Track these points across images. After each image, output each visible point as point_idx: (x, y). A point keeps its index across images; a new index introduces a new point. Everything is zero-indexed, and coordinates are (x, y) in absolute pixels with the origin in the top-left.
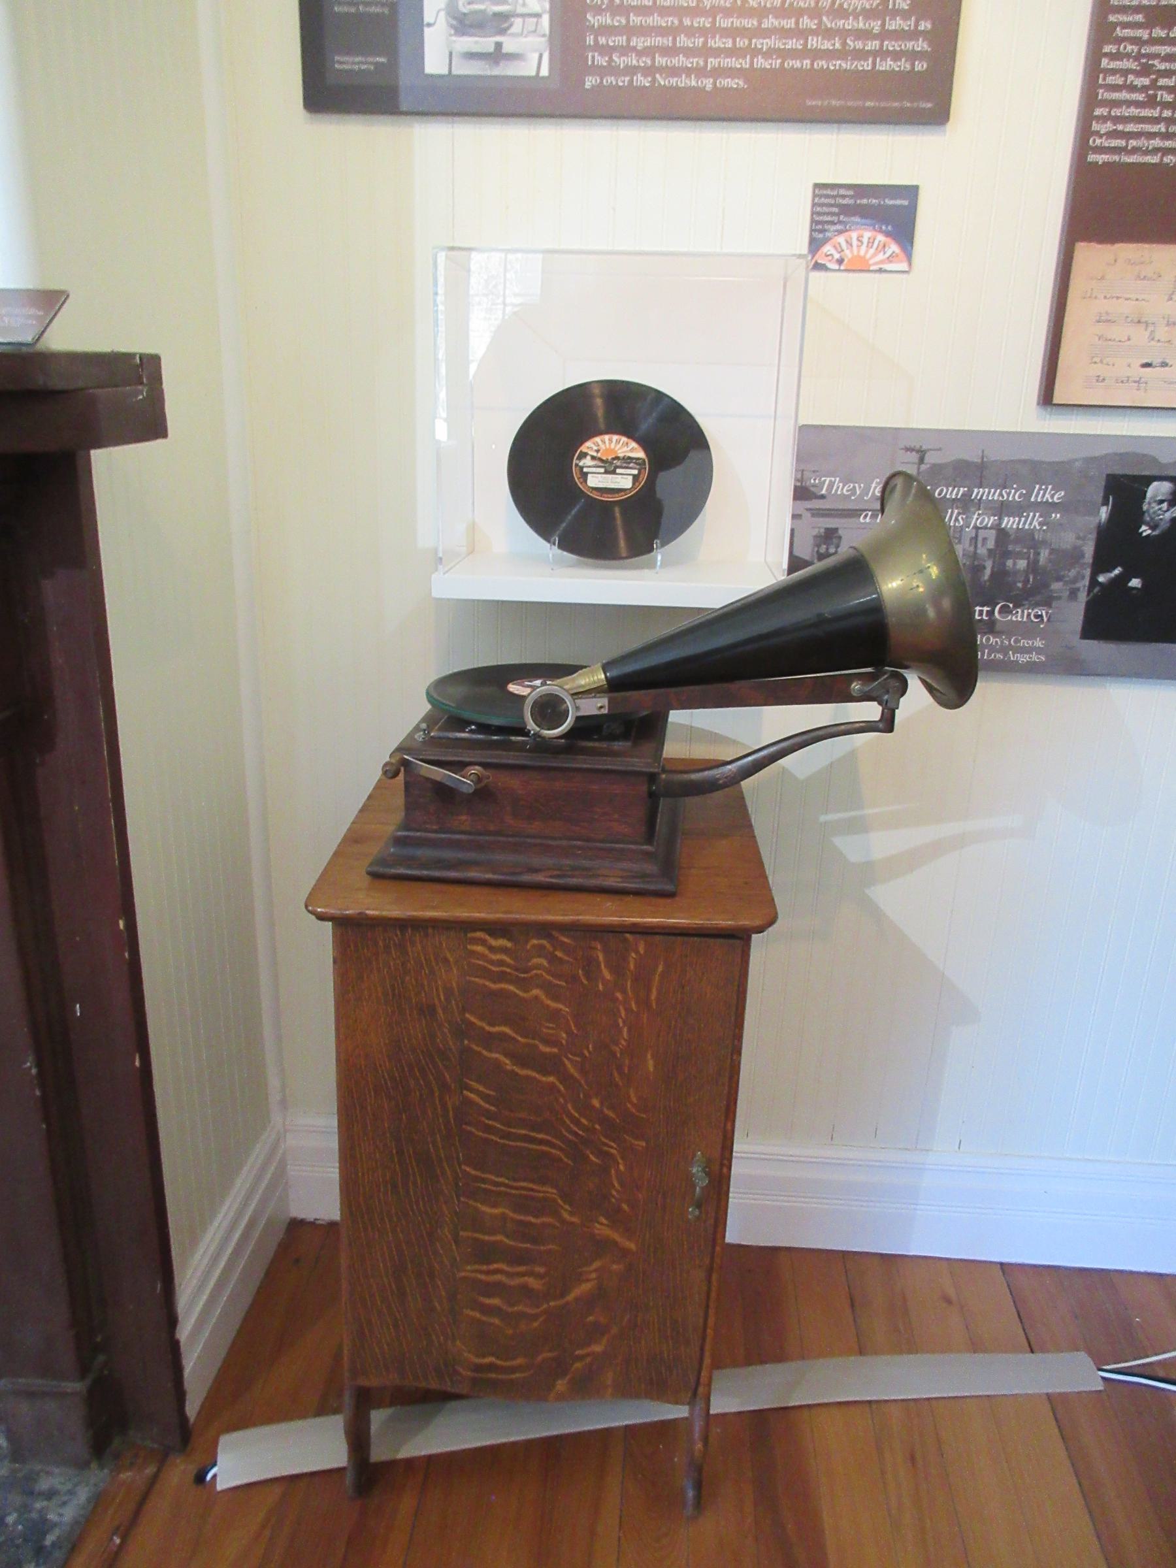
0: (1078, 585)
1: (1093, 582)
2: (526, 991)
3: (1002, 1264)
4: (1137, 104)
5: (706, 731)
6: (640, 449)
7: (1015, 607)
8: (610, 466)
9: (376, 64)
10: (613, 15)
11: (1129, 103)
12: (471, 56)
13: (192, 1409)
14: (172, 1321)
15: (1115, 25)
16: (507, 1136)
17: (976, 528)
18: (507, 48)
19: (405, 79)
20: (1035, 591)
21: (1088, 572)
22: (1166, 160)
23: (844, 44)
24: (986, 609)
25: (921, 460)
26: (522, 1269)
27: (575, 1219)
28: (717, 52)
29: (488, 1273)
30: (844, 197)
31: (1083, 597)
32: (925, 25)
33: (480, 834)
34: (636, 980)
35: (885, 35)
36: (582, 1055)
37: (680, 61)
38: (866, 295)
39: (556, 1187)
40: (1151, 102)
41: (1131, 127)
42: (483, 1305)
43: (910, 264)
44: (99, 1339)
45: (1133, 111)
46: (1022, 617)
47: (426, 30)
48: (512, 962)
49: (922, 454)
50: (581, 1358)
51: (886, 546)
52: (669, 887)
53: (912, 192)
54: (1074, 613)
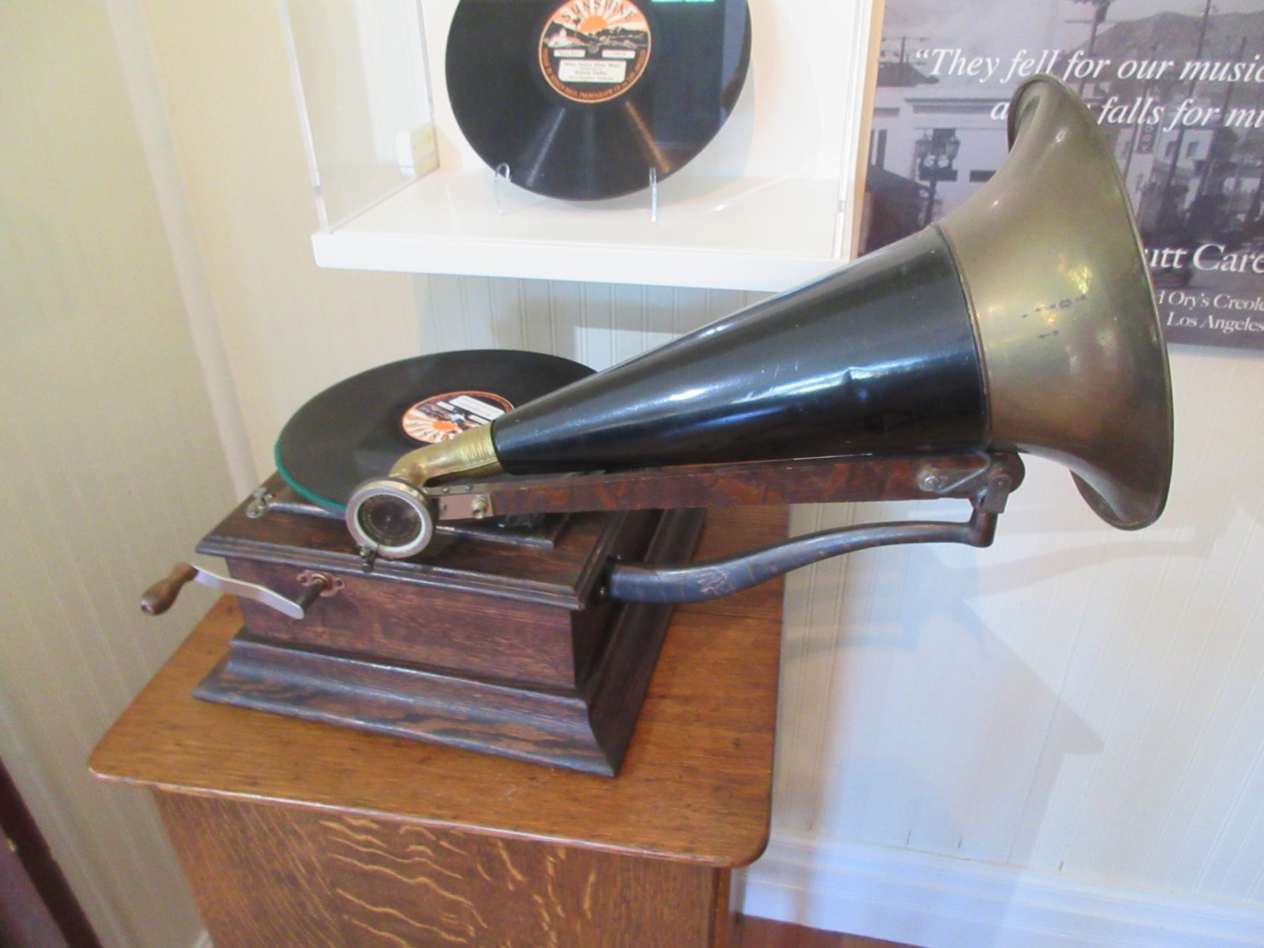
6: (642, 17)
17: (1181, 128)
24: (1179, 253)
34: (559, 887)
46: (1238, 265)
48: (385, 846)
51: (997, 237)
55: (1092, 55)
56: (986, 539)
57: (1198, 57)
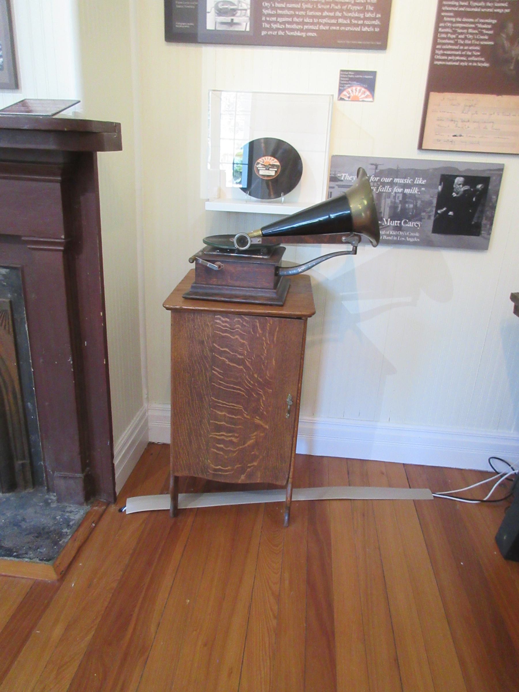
0: (431, 214)
1: (436, 213)
2: (234, 336)
3: (404, 464)
4: (451, 44)
5: (297, 255)
8: (268, 167)
9: (190, 26)
10: (272, 10)
12: (223, 23)
13: (118, 490)
14: (112, 456)
15: (443, 17)
16: (227, 387)
17: (395, 193)
18: (235, 21)
19: (200, 32)
20: (416, 216)
21: (434, 209)
23: (351, 21)
25: (376, 168)
26: (230, 434)
27: (248, 417)
28: (307, 24)
29: (219, 435)
30: (350, 75)
31: (433, 218)
32: (379, 16)
33: (219, 285)
34: (269, 333)
35: (365, 19)
36: (251, 359)
37: (294, 26)
39: (242, 405)
40: (456, 44)
41: (449, 52)
42: (217, 447)
43: (373, 98)
44: (88, 461)
47: (208, 15)
49: (377, 166)
50: (250, 467)
52: (281, 303)
53: (374, 73)
54: (430, 224)
55: (376, 176)
56: (355, 253)
57: (397, 178)
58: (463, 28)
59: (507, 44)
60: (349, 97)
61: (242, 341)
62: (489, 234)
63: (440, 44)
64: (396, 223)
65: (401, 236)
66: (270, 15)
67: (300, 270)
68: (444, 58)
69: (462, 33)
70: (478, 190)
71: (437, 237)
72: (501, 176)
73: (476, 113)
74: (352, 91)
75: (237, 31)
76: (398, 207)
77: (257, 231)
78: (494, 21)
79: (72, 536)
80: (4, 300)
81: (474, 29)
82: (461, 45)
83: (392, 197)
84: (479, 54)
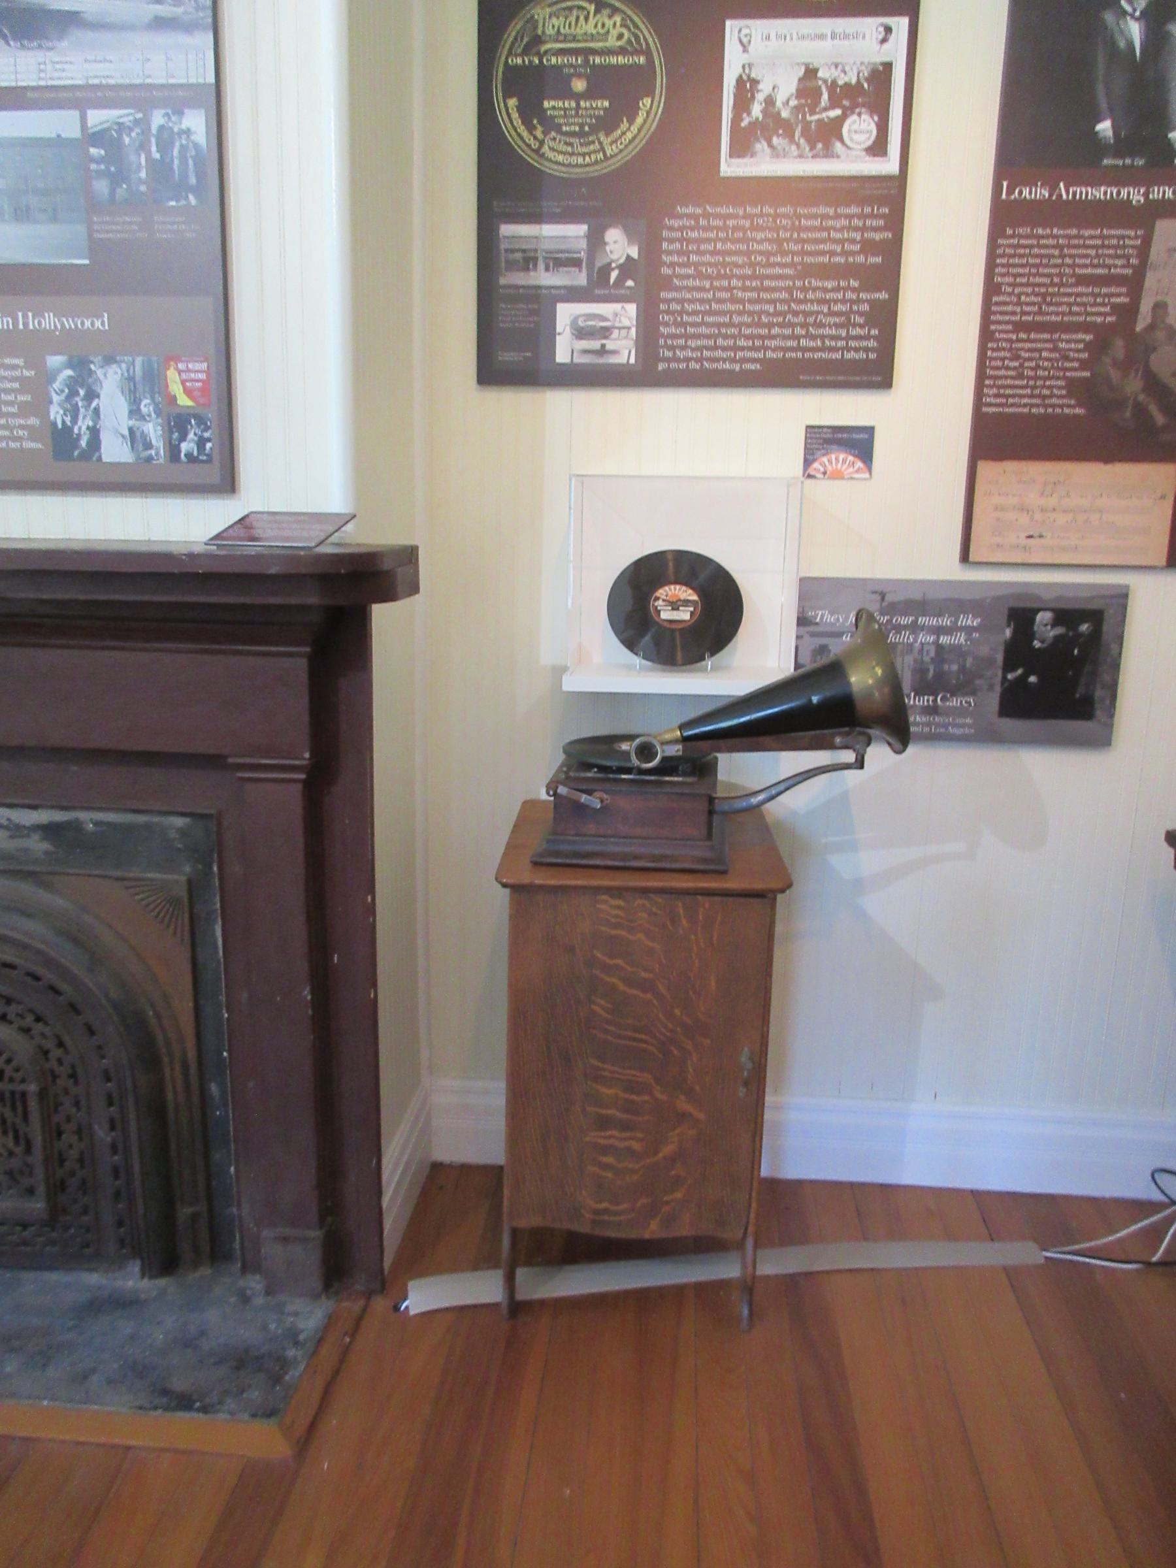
1: (1004, 678)
4: (1012, 378)
5: (744, 770)
7: (952, 696)
11: (1006, 377)
12: (586, 352)
13: (387, 1263)
14: (379, 1193)
15: (993, 332)
16: (620, 1037)
20: (964, 685)
22: (1034, 410)
23: (823, 343)
25: (883, 599)
26: (628, 1134)
28: (742, 349)
29: (605, 1137)
31: (998, 689)
35: (849, 337)
37: (719, 354)
38: (843, 492)
40: (1021, 376)
45: (1009, 382)
47: (558, 337)
49: (883, 596)
50: (667, 1203)
53: (870, 430)
54: (993, 701)
56: (862, 767)
58: (1029, 350)
59: (1115, 375)
60: (825, 473)
61: (649, 944)
62: (1112, 716)
63: (991, 377)
64: (927, 700)
65: (938, 725)
66: (674, 336)
67: (754, 800)
68: (998, 401)
69: (1030, 359)
70: (1081, 635)
71: (1008, 724)
72: (1124, 607)
73: (1068, 495)
74: (830, 462)
75: (615, 365)
76: (928, 670)
77: (672, 730)
78: (1088, 337)
79: (308, 1365)
80: (176, 877)
81: (1050, 350)
82: (1029, 378)
83: (916, 651)
84: (1064, 392)
